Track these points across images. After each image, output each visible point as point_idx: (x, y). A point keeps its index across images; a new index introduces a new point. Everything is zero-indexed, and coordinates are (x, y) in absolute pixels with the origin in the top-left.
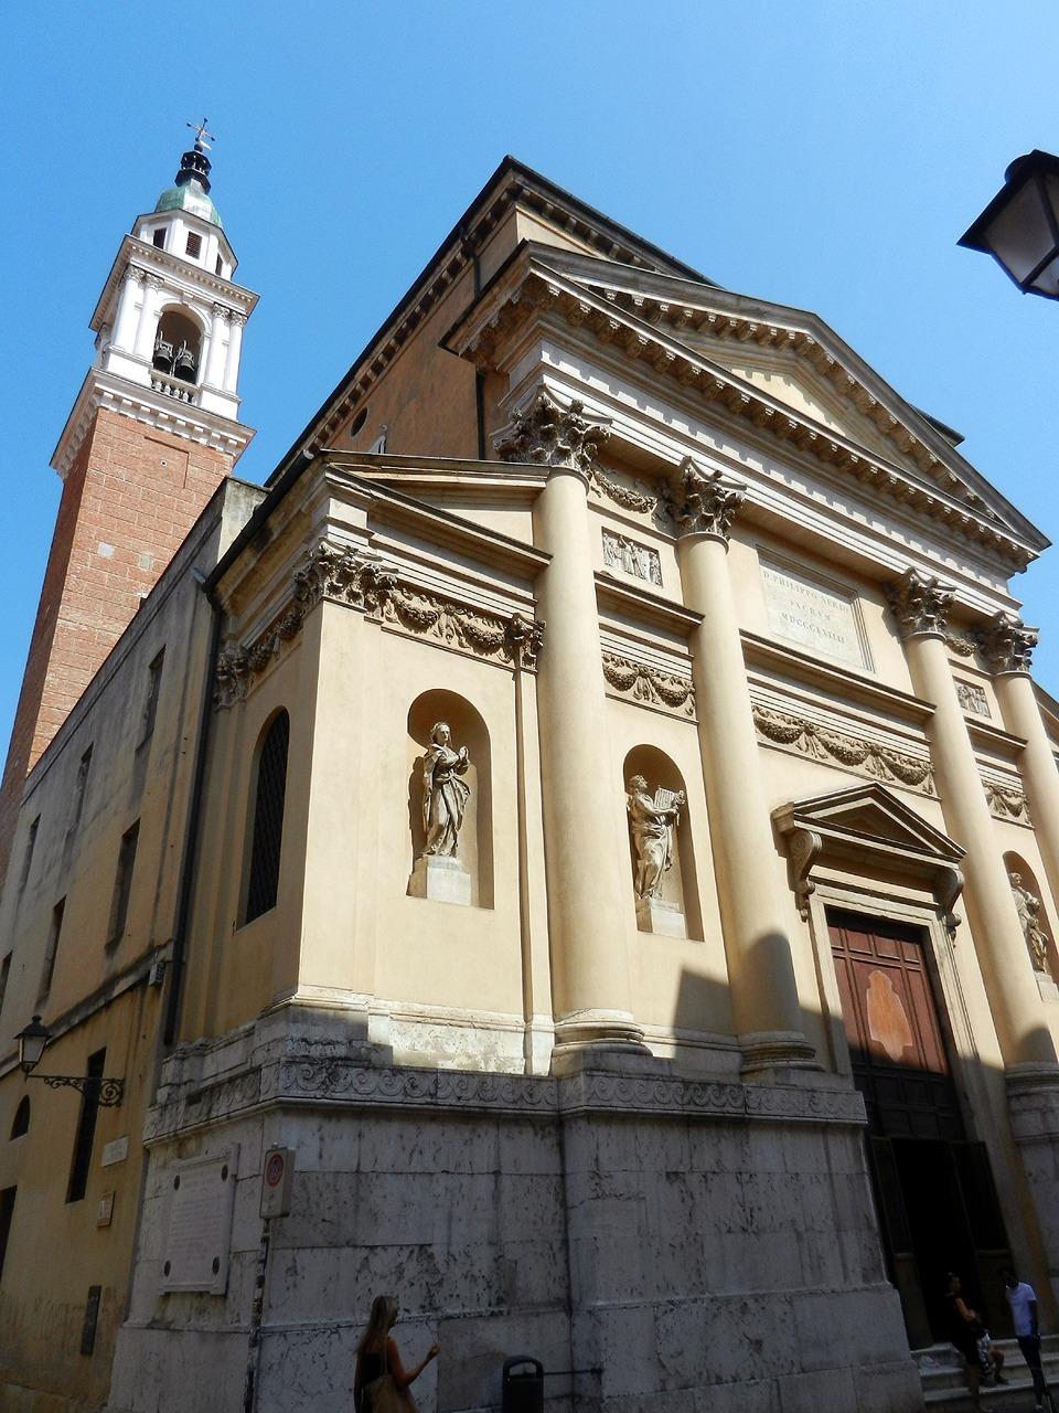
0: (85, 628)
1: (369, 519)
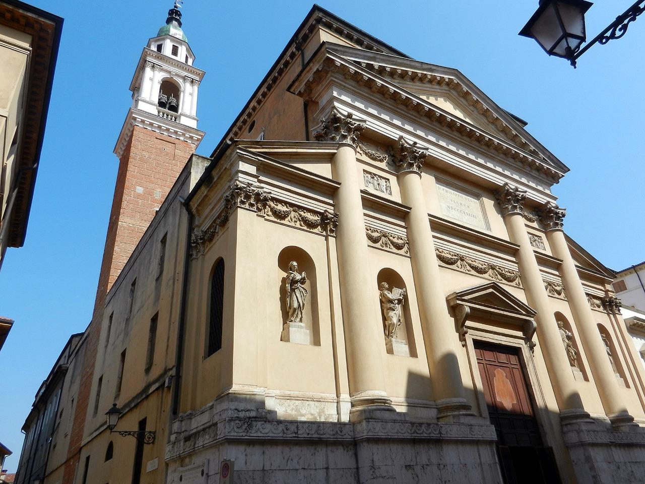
0: (131, 225)
1: (257, 170)
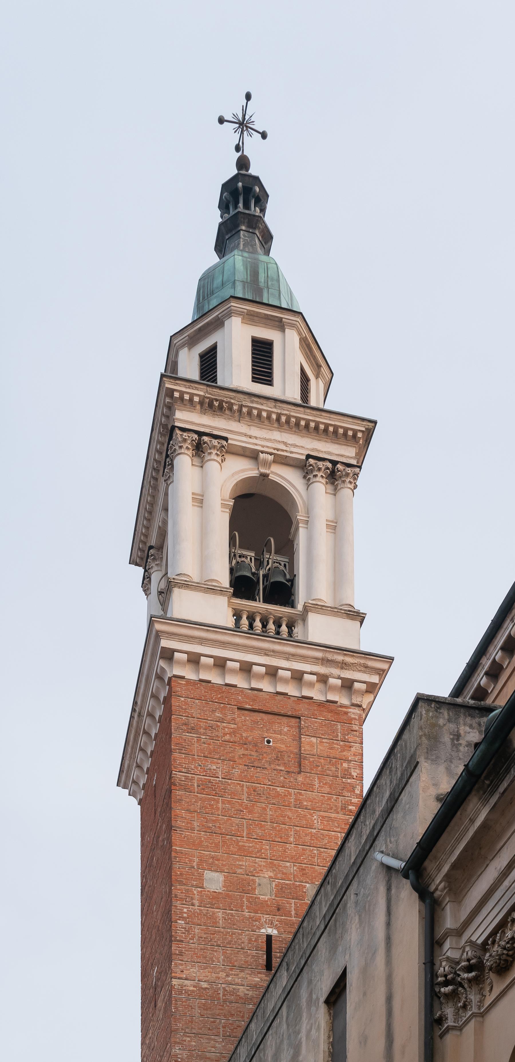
0: (205, 985)
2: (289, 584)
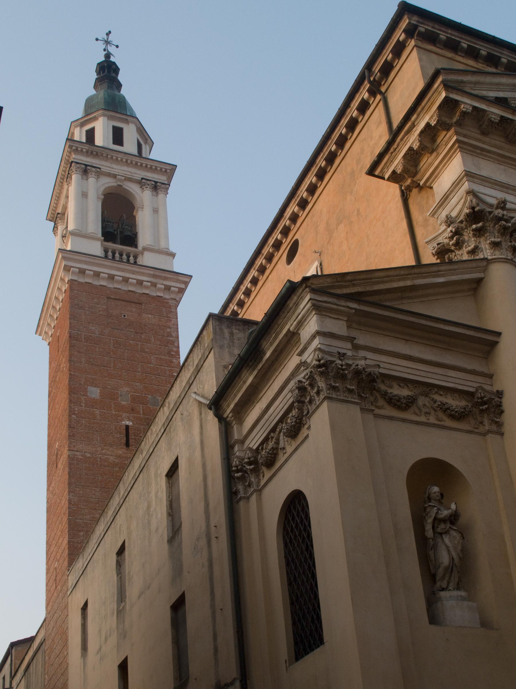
0: (88, 455)
1: (349, 327)
2: (134, 236)
